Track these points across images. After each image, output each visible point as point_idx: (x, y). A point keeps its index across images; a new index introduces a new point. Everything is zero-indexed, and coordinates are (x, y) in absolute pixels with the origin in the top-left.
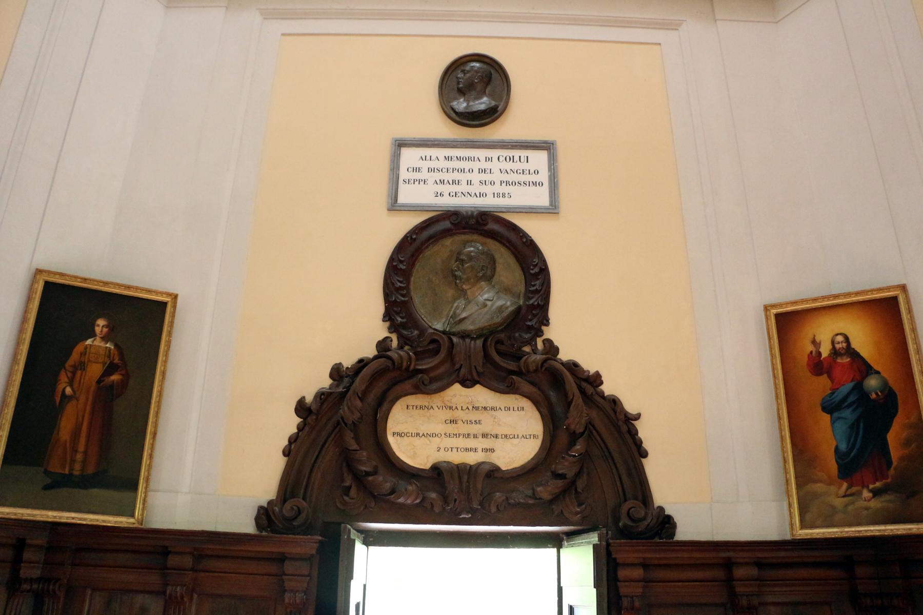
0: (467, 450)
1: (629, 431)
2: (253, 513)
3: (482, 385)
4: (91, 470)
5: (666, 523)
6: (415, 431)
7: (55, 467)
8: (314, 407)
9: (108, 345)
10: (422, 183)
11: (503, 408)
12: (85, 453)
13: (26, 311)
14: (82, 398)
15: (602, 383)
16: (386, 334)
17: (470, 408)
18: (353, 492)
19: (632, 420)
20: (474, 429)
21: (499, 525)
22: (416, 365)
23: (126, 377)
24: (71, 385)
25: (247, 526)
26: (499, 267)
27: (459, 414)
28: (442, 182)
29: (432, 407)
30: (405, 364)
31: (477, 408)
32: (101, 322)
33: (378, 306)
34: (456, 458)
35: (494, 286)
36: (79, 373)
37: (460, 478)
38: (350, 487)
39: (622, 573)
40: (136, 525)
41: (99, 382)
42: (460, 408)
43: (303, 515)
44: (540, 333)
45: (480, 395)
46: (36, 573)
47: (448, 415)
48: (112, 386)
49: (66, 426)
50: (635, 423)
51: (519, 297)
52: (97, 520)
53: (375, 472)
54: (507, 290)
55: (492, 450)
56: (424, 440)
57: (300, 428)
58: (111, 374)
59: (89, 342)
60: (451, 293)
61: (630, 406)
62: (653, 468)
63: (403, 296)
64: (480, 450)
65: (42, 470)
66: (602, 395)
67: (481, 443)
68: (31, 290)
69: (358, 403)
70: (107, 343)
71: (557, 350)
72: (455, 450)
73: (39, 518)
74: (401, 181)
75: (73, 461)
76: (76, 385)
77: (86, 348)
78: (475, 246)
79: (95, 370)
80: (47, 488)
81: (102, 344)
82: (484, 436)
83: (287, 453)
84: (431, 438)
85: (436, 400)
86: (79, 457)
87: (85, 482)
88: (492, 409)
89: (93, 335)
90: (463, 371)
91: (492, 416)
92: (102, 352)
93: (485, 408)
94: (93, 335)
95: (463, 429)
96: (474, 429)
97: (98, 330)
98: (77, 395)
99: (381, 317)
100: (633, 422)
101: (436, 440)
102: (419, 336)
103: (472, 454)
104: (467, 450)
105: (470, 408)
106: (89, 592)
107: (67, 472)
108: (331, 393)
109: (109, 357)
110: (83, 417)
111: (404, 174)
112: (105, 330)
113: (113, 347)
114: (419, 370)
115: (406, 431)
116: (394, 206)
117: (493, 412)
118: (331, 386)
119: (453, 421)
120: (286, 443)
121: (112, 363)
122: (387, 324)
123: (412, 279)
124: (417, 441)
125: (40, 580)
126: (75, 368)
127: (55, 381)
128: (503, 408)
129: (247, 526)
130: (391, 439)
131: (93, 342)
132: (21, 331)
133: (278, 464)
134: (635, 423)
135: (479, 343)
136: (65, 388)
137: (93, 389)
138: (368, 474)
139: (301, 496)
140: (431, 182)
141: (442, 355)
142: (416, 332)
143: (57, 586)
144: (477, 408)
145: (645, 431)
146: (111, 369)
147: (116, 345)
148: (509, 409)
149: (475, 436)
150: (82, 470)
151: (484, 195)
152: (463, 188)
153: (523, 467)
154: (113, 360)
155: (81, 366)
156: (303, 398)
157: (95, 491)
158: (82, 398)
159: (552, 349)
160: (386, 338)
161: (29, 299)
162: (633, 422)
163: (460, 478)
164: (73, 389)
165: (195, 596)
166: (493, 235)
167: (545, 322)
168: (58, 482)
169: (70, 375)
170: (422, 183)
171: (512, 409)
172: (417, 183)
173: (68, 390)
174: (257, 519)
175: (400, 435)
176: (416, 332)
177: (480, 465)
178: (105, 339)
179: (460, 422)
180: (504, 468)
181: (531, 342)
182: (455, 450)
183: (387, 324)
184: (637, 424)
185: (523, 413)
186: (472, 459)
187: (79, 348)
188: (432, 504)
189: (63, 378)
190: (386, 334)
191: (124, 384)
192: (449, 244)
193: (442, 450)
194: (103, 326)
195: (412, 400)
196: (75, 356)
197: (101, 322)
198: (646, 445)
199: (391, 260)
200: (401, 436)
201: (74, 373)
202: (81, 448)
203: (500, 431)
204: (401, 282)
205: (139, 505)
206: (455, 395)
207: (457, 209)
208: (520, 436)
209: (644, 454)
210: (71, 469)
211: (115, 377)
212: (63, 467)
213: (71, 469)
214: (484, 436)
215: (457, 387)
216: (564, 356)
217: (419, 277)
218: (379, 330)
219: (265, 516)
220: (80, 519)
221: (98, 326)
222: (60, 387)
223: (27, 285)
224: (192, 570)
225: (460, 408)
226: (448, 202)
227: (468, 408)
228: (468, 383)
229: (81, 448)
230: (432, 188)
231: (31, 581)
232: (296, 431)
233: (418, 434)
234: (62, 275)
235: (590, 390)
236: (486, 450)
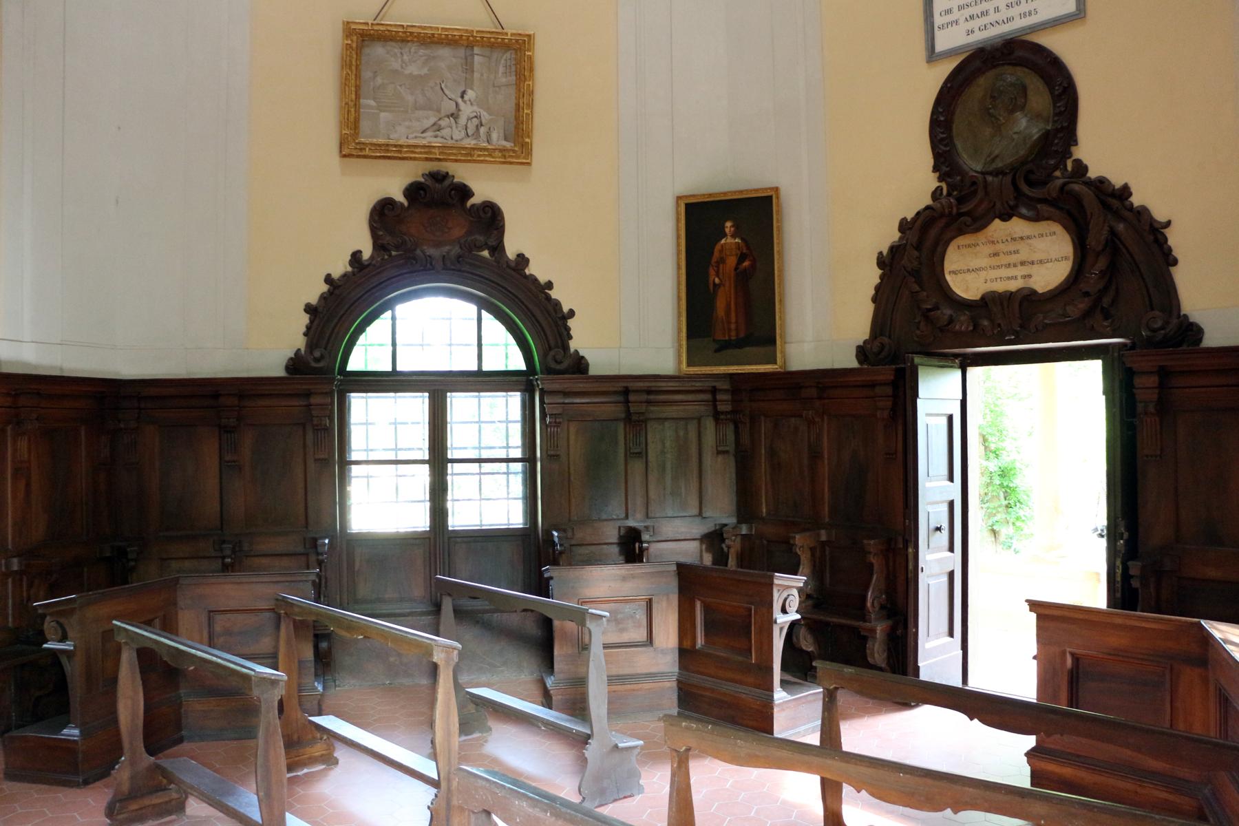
0: (1009, 278)
1: (1156, 241)
2: (854, 352)
3: (1017, 216)
4: (742, 335)
5: (1192, 332)
6: (966, 268)
7: (719, 336)
8: (887, 261)
9: (737, 241)
10: (954, 25)
11: (1037, 235)
12: (736, 322)
13: (678, 230)
14: (727, 284)
15: (1130, 194)
16: (938, 184)
17: (1009, 240)
18: (922, 324)
19: (1162, 228)
20: (1014, 258)
21: (1040, 343)
22: (958, 209)
23: (754, 261)
24: (718, 276)
25: (851, 362)
26: (1030, 94)
27: (1001, 247)
28: (972, 17)
29: (978, 244)
30: (947, 211)
31: (1014, 239)
32: (728, 224)
33: (928, 160)
34: (1000, 287)
35: (1026, 116)
36: (721, 266)
37: (1002, 304)
38: (919, 322)
39: (1138, 381)
40: (779, 370)
41: (736, 269)
42: (1000, 241)
43: (886, 349)
44: (1070, 155)
45: (1017, 226)
46: (728, 408)
47: (988, 249)
48: (745, 269)
49: (720, 305)
50: (1166, 231)
51: (1048, 121)
52: (752, 369)
53: (936, 308)
54: (1038, 116)
55: (1030, 276)
56: (973, 275)
57: (882, 277)
58: (743, 262)
59: (723, 241)
60: (988, 131)
61: (1160, 215)
62: (1182, 276)
63: (946, 146)
64: (1019, 278)
65: (711, 339)
66: (1131, 208)
67: (1020, 271)
68: (678, 213)
69: (916, 253)
70: (735, 239)
71: (1086, 169)
72: (999, 280)
73: (715, 372)
74: (936, 28)
75: (730, 330)
76: (721, 276)
77: (722, 246)
78: (1011, 75)
79: (732, 261)
80: (717, 351)
81: (732, 241)
82: (1023, 263)
83: (874, 300)
84: (978, 272)
85: (981, 237)
86: (733, 326)
87: (740, 343)
88: (1029, 238)
89: (725, 235)
90: (998, 205)
91: (1028, 244)
92: (734, 247)
93: (1022, 238)
94: (725, 235)
95: (1004, 260)
96: (1014, 258)
97: (727, 230)
98: (723, 283)
99: (931, 169)
100: (1162, 230)
101: (983, 274)
102: (962, 181)
103: (1013, 281)
104: (1009, 278)
105: (1009, 240)
106: (763, 418)
107: (727, 338)
108: (900, 245)
109: (739, 249)
110: (730, 298)
111: (938, 20)
112: (732, 229)
113: (740, 241)
114: (963, 213)
115: (959, 269)
116: (932, 55)
117: (1029, 241)
118: (901, 239)
119: (996, 254)
120: (873, 292)
121: (742, 253)
122: (937, 174)
123: (954, 126)
124: (969, 277)
125: (732, 412)
126: (718, 263)
127: (707, 274)
128: (1037, 235)
129: (851, 362)
130: (948, 277)
131: (726, 240)
132: (678, 245)
133: (868, 309)
134: (1166, 231)
135: (1008, 179)
136: (714, 280)
137: (732, 276)
138: (929, 310)
139: (887, 334)
140: (962, 21)
141: (980, 194)
142: (959, 178)
143: (741, 416)
144: (1014, 239)
145: (1176, 239)
146: (742, 258)
147: (742, 239)
148: (1042, 236)
149: (1015, 266)
150: (737, 336)
151: (1011, 19)
152: (992, 17)
153: (1056, 288)
154: (743, 249)
155: (722, 260)
156: (881, 253)
157: (747, 349)
158: (727, 284)
159: (1081, 168)
160: (938, 187)
161: (678, 220)
162: (1162, 230)
163: (1002, 304)
164: (720, 279)
165: (826, 418)
166: (1021, 63)
167: (905, 222)
168: (724, 346)
169: (715, 269)
170: (954, 25)
171: (1044, 235)
172: (950, 26)
173: (717, 280)
174: (857, 356)
175: (954, 272)
176: (959, 178)
177: (1019, 290)
178: (733, 236)
179: (1001, 254)
180: (1040, 291)
181: (1062, 163)
182: (999, 280)
183: (937, 174)
184: (1167, 232)
185: (1054, 237)
186: (1013, 286)
187: (718, 247)
188: (983, 330)
189: (712, 272)
190: (938, 184)
191: (753, 266)
192: (983, 82)
193: (989, 282)
194: (730, 227)
195: (961, 240)
196: (716, 254)
197: (728, 224)
198: (1176, 252)
199: (933, 113)
200: (956, 274)
201: (718, 267)
202: (733, 320)
203: (1036, 257)
204: (943, 133)
205: (779, 355)
206: (995, 230)
207: (980, 46)
208: (1053, 259)
209: (1175, 262)
210: (730, 336)
211: (746, 264)
212: (725, 337)
213: (730, 336)
214: (1023, 263)
215: (997, 221)
216: (1093, 174)
217: (959, 125)
218: (930, 182)
219: (862, 352)
220: (740, 370)
221: (727, 227)
222: (711, 282)
223: (674, 210)
224: (820, 398)
225: (1000, 241)
226: (979, 37)
227: (1007, 240)
228: (1006, 217)
229: (733, 320)
230: (964, 26)
231: (727, 413)
232: (879, 281)
233: (968, 270)
234: (693, 196)
235: (1115, 203)
236: (1024, 277)
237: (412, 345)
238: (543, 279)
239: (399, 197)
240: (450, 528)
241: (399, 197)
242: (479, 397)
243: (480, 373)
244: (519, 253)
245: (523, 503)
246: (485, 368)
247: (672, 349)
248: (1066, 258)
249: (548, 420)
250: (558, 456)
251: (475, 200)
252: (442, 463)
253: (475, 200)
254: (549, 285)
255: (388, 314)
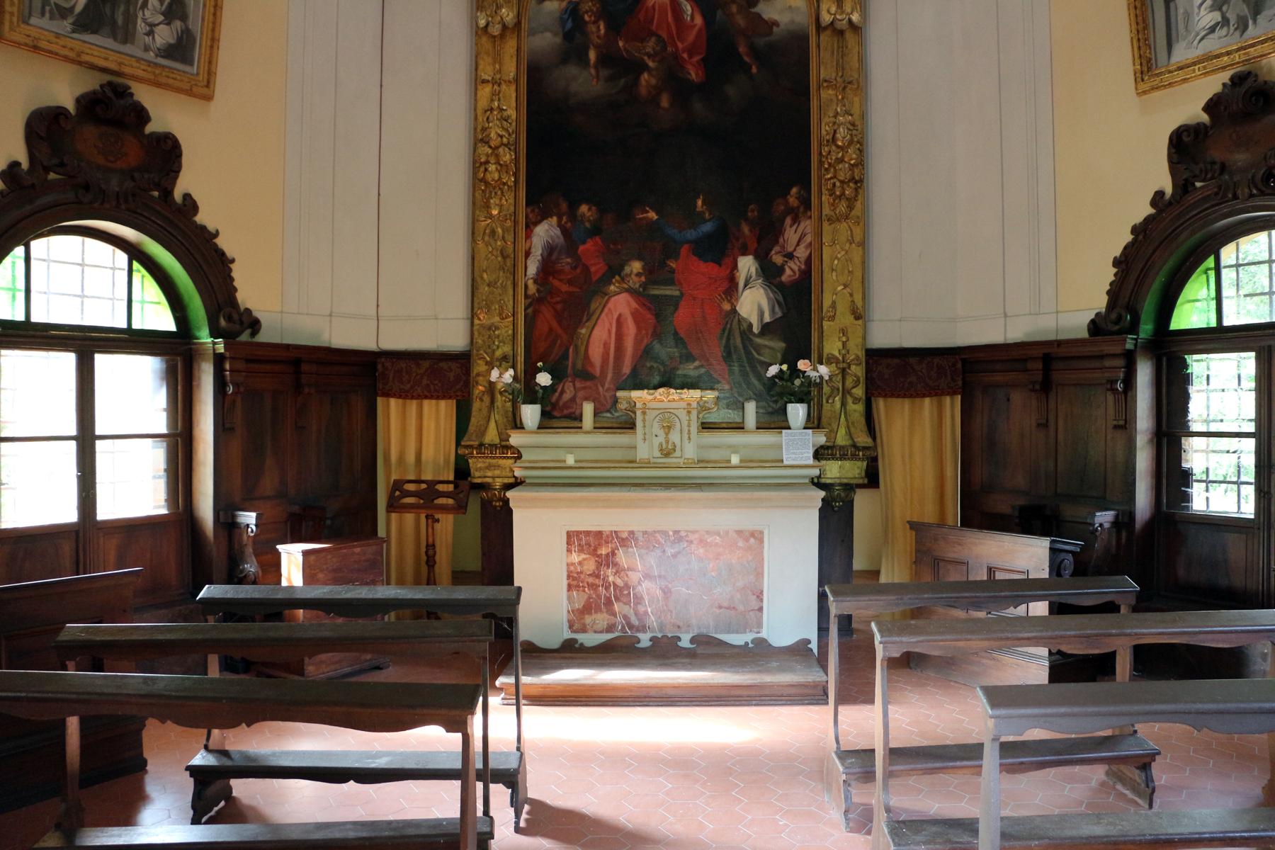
174: (1089, 329)
237: (83, 286)
238: (211, 227)
239: (70, 105)
240: (164, 511)
241: (70, 105)
242: (1005, 339)
243: (129, 330)
244: (186, 192)
245: (1256, 394)
246: (1227, 322)
247: (875, 319)
248: (114, 250)
249: (230, 389)
250: (233, 429)
251: (150, 128)
252: (83, 436)
253: (150, 128)
254: (217, 234)
255: (19, 251)
